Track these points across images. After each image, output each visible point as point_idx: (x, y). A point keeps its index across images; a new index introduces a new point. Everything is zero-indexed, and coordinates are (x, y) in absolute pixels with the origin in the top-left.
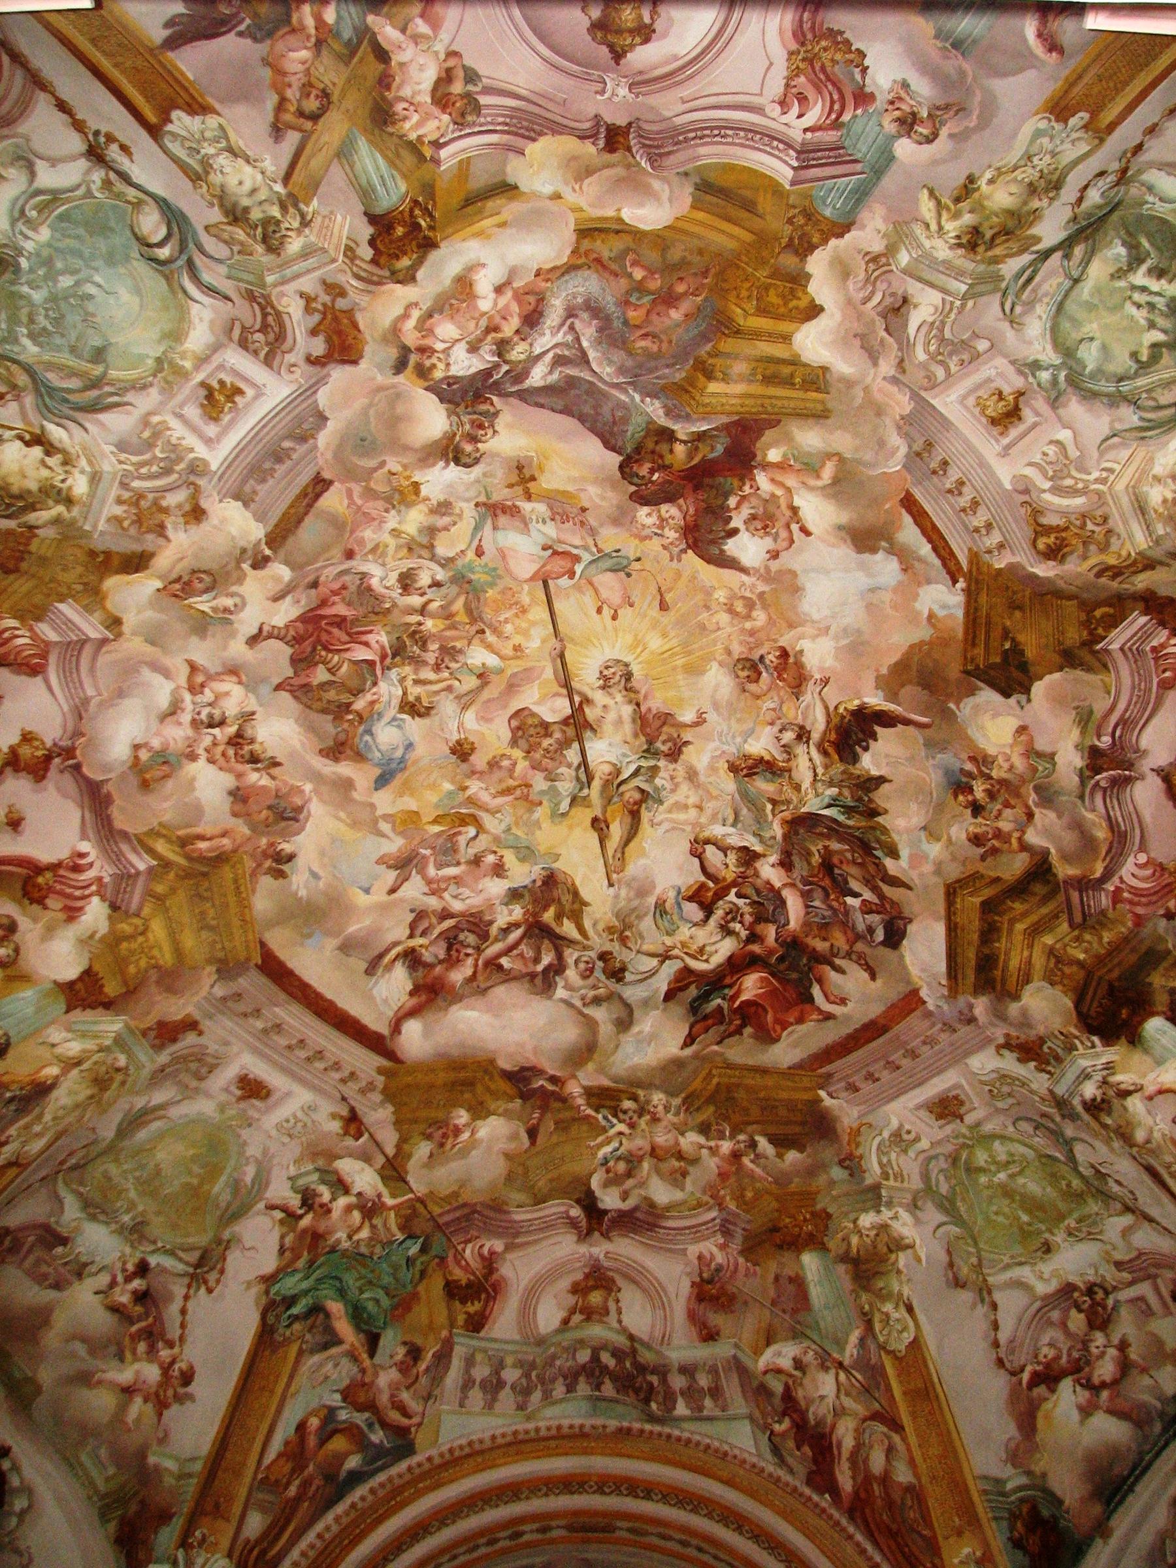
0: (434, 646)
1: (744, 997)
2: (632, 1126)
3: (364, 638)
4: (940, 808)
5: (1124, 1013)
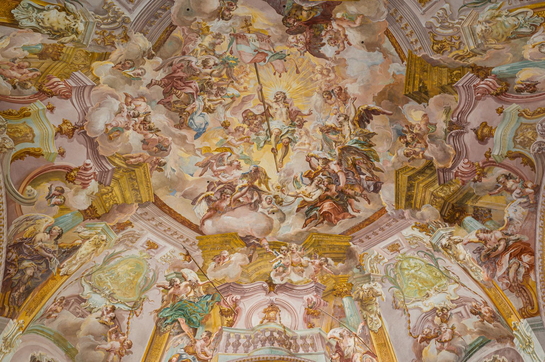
0: (215, 87)
1: (324, 210)
2: (285, 255)
3: (190, 84)
4: (394, 143)
5: (457, 215)
